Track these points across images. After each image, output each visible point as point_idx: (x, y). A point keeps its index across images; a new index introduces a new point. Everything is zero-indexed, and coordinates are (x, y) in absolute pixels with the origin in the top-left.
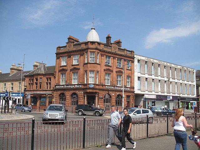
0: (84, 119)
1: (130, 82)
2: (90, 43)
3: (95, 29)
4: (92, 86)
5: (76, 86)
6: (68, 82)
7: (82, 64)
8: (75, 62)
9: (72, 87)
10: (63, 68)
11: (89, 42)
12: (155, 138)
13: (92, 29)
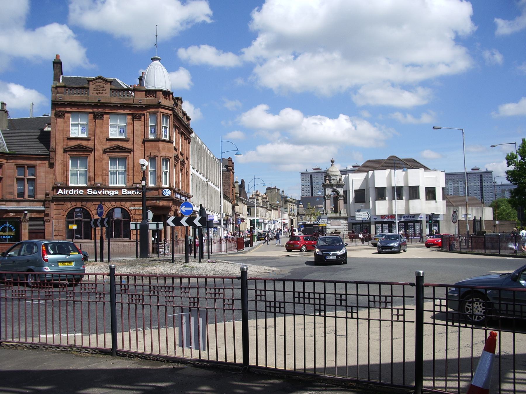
0: (81, 244)
1: (168, 174)
2: (161, 93)
3: (159, 60)
4: (168, 193)
5: (124, 192)
6: (99, 180)
7: (139, 140)
8: (114, 133)
9: (112, 193)
10: (79, 142)
11: (160, 90)
12: (293, 309)
13: (153, 59)
